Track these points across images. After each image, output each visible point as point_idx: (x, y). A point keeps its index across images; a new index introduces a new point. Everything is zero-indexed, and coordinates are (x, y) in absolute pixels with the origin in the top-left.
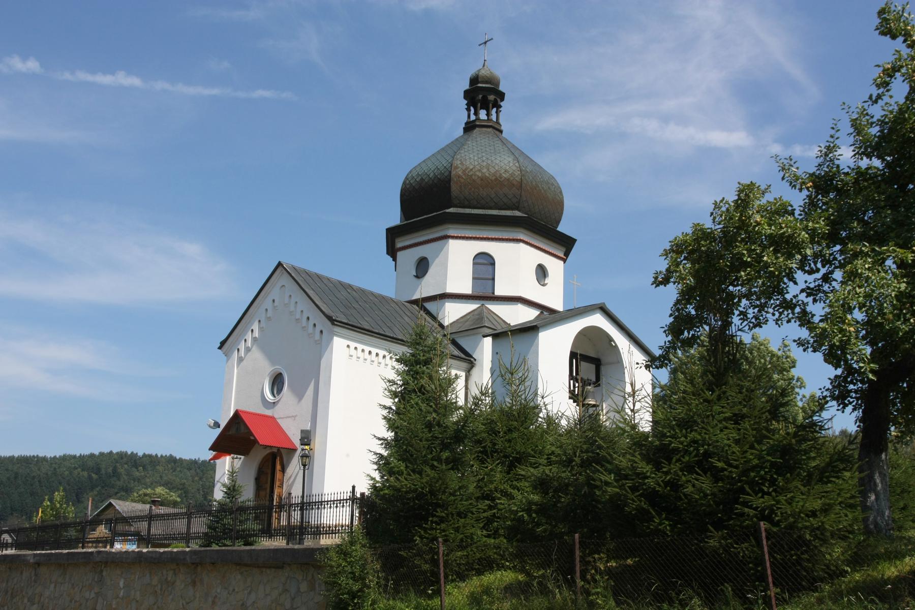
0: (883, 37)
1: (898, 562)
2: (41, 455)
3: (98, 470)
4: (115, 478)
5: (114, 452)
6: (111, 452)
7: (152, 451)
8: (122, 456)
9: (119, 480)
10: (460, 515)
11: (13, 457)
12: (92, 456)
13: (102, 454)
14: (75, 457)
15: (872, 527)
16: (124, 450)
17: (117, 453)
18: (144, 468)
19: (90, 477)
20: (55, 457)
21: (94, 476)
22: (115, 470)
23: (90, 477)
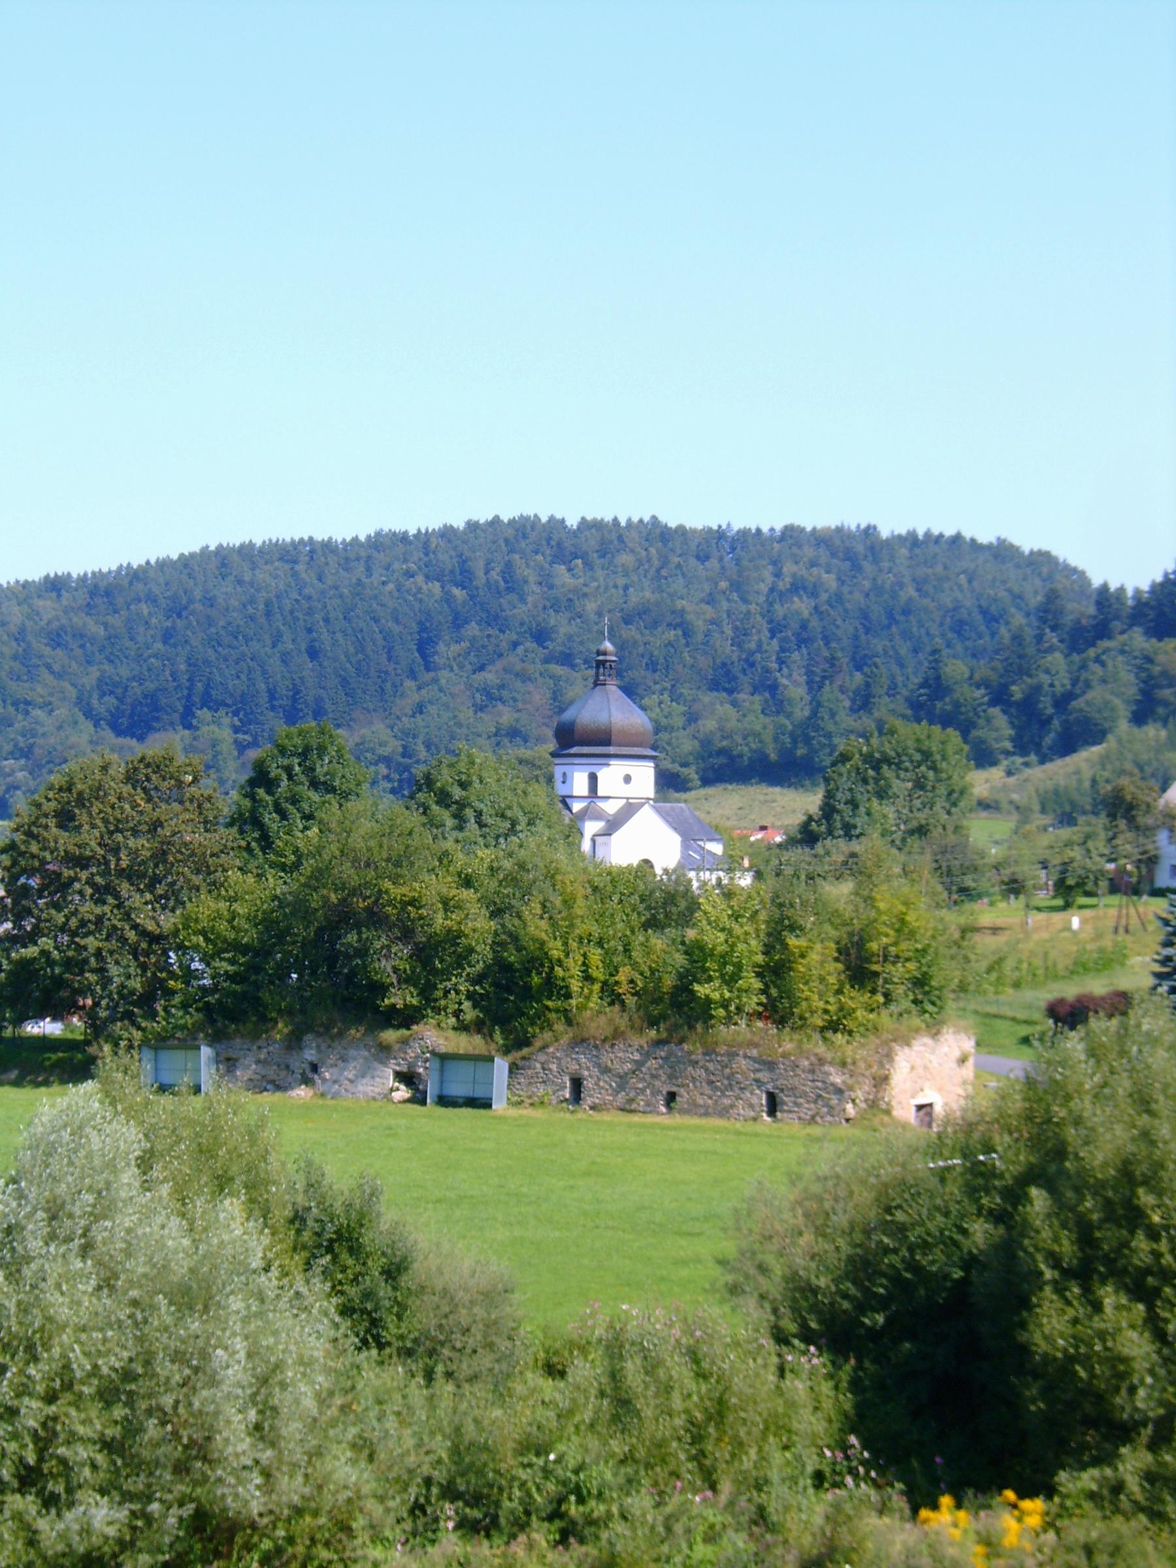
0: (443, 1110)
1: (729, 1248)
2: (320, 536)
3: (464, 577)
4: (513, 597)
5: (505, 518)
6: (496, 521)
7: (603, 512)
8: (524, 528)
9: (523, 600)
10: (361, 648)
11: (251, 545)
12: (447, 533)
13: (472, 526)
14: (404, 538)
15: (238, 988)
16: (529, 511)
17: (512, 522)
18: (588, 565)
19: (448, 599)
20: (355, 539)
21: (457, 592)
22: (508, 571)
23: (448, 599)
